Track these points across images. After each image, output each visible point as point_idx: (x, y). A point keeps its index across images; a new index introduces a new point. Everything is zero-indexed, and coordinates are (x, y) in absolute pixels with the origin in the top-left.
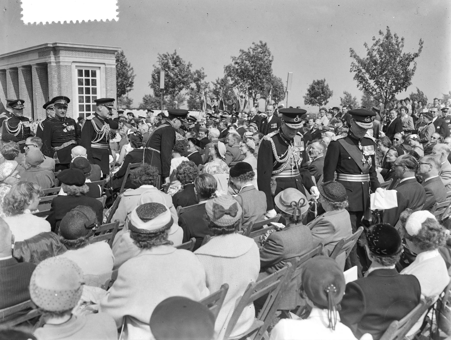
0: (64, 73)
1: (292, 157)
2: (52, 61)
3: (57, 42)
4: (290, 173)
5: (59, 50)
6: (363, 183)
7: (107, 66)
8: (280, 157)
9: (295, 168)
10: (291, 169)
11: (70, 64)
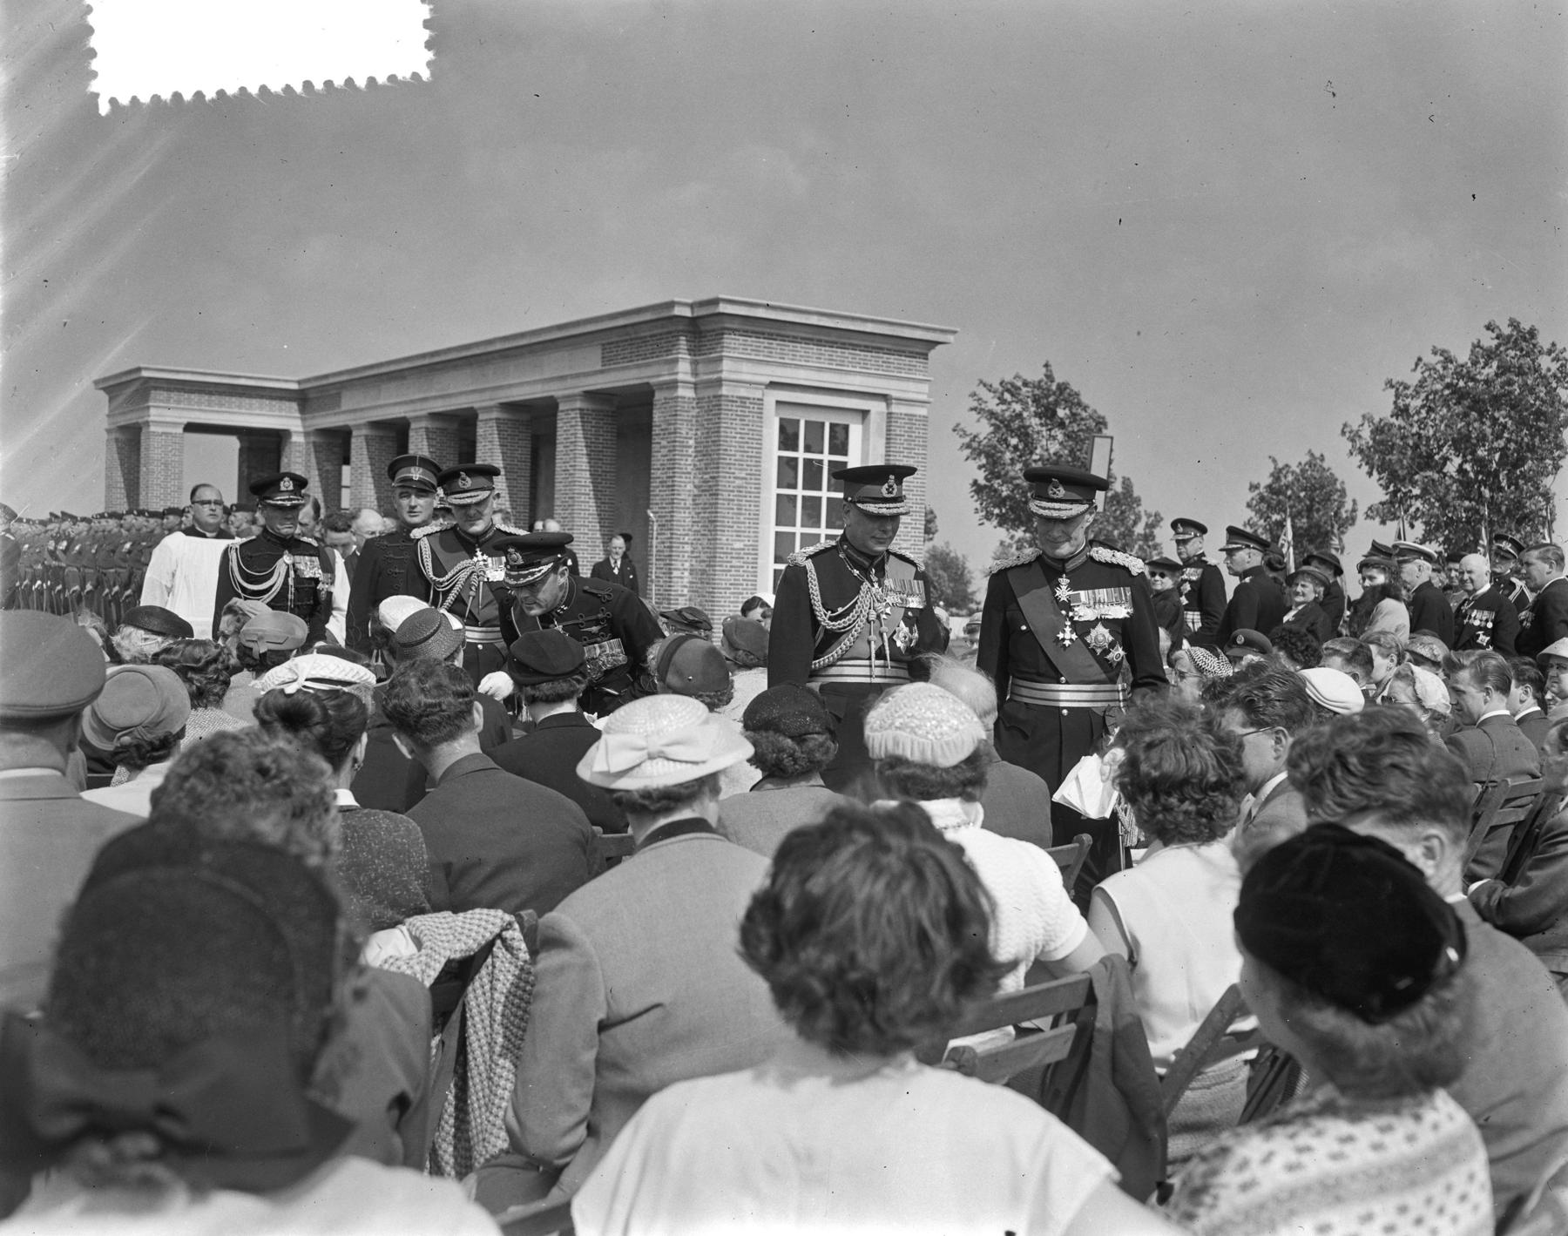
1: (873, 616)
2: (680, 377)
3: (722, 296)
4: (866, 671)
5: (720, 334)
6: (1065, 712)
7: (895, 409)
9: (880, 655)
11: (758, 394)
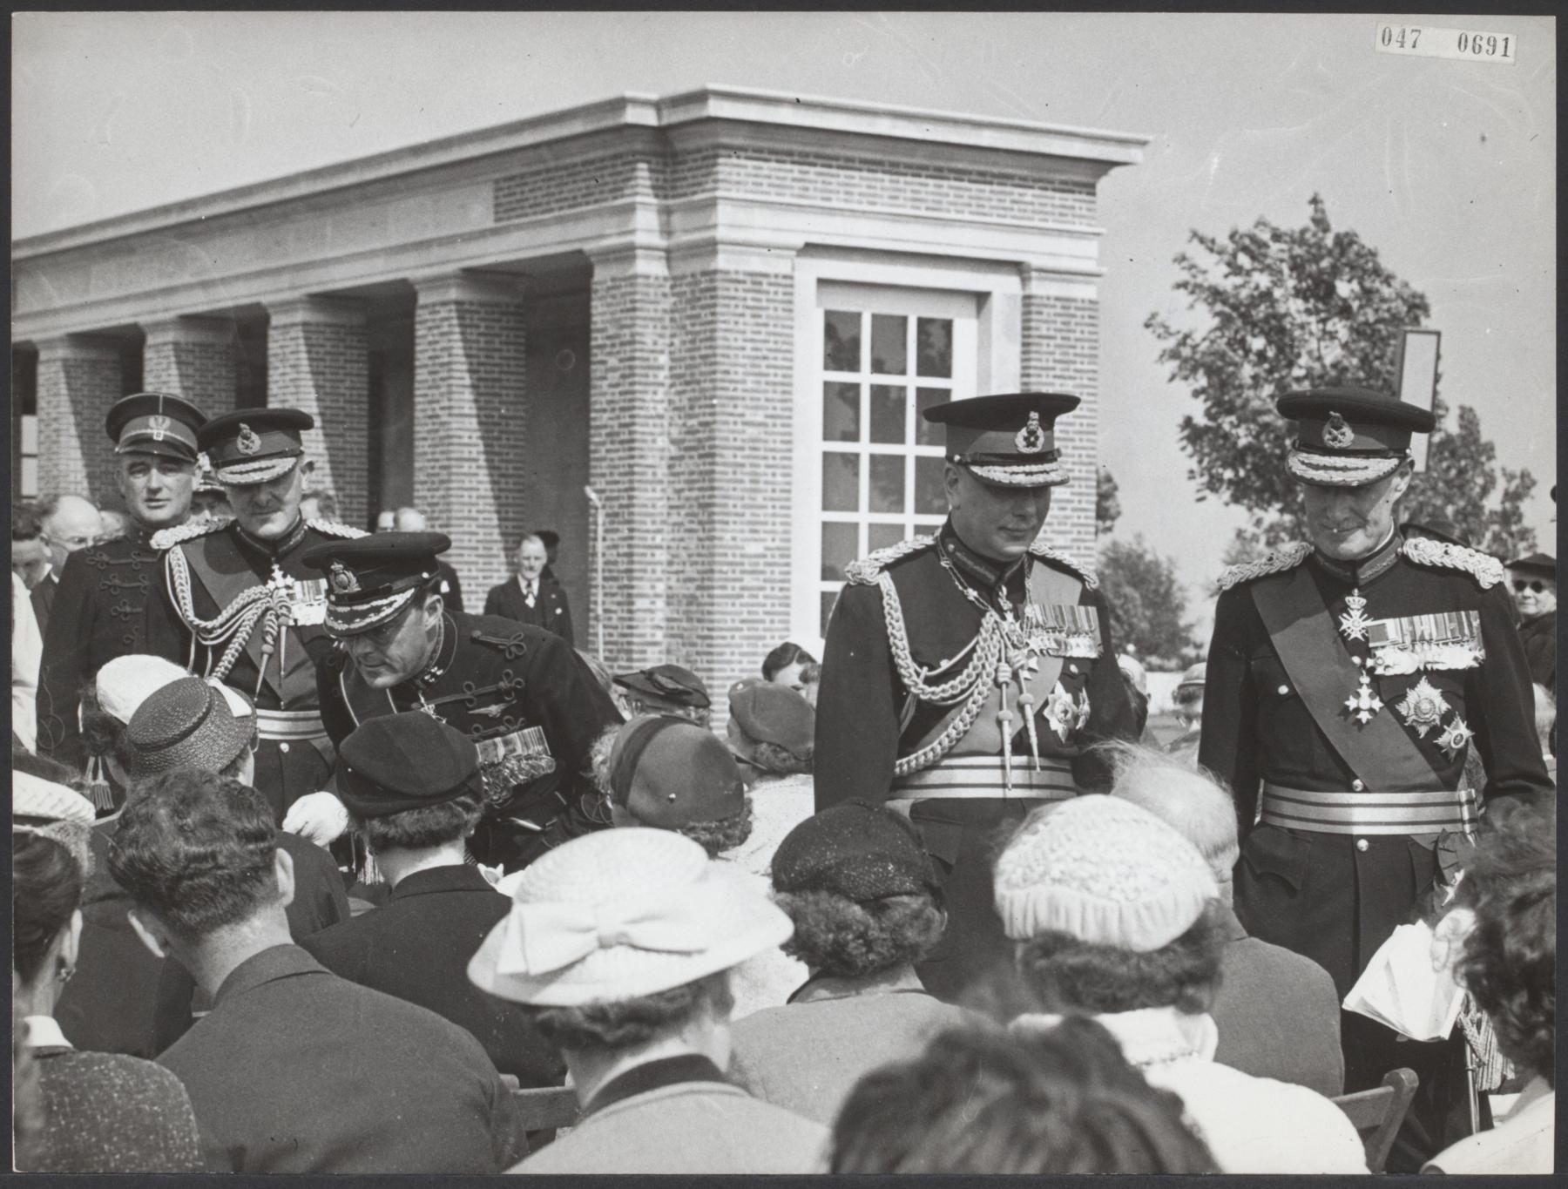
0: (735, 333)
2: (640, 238)
4: (995, 776)
5: (710, 157)
7: (1038, 288)
8: (924, 671)
9: (1021, 745)
10: (1001, 753)
11: (782, 267)
